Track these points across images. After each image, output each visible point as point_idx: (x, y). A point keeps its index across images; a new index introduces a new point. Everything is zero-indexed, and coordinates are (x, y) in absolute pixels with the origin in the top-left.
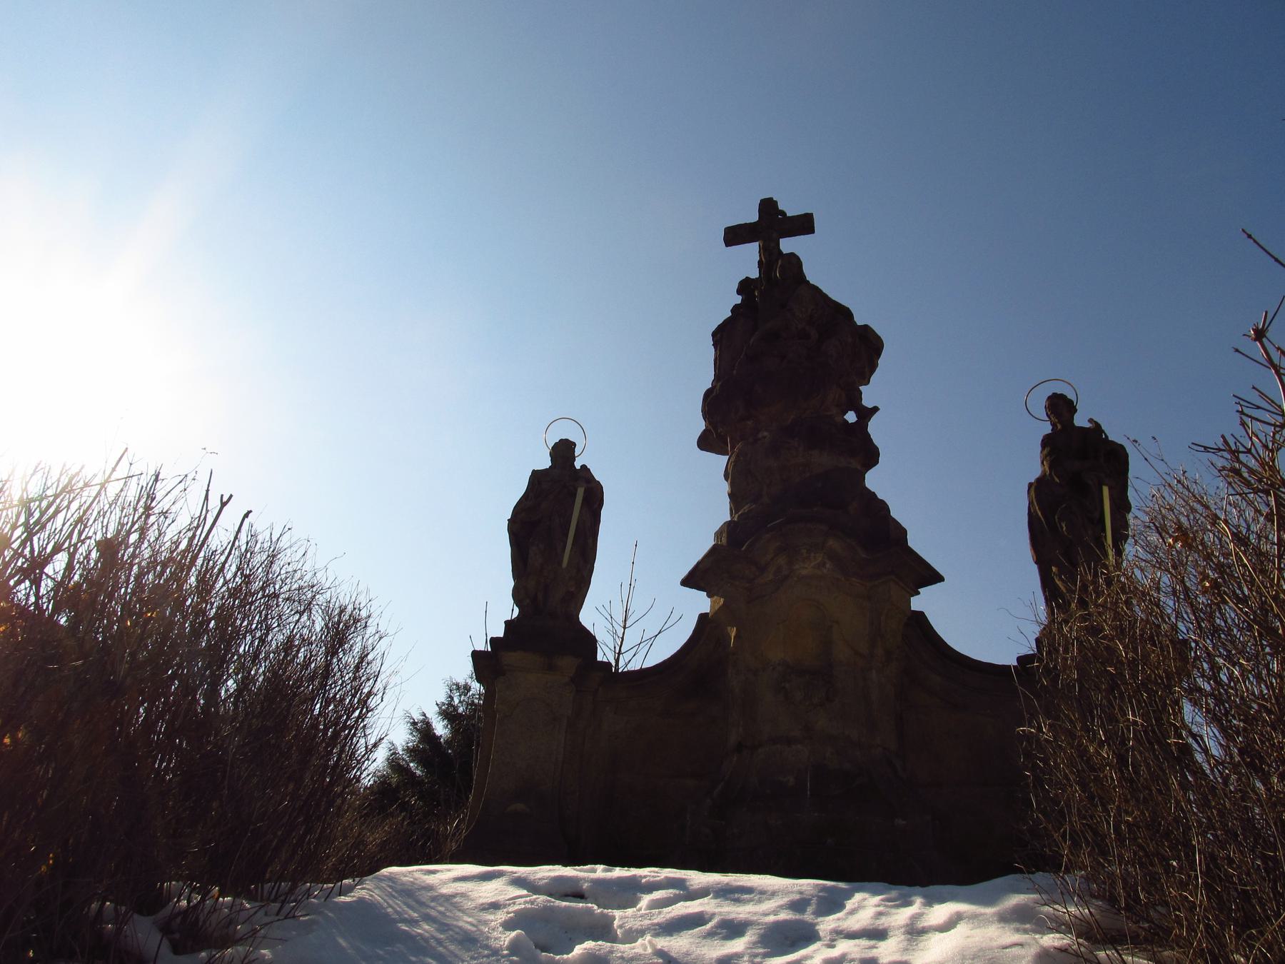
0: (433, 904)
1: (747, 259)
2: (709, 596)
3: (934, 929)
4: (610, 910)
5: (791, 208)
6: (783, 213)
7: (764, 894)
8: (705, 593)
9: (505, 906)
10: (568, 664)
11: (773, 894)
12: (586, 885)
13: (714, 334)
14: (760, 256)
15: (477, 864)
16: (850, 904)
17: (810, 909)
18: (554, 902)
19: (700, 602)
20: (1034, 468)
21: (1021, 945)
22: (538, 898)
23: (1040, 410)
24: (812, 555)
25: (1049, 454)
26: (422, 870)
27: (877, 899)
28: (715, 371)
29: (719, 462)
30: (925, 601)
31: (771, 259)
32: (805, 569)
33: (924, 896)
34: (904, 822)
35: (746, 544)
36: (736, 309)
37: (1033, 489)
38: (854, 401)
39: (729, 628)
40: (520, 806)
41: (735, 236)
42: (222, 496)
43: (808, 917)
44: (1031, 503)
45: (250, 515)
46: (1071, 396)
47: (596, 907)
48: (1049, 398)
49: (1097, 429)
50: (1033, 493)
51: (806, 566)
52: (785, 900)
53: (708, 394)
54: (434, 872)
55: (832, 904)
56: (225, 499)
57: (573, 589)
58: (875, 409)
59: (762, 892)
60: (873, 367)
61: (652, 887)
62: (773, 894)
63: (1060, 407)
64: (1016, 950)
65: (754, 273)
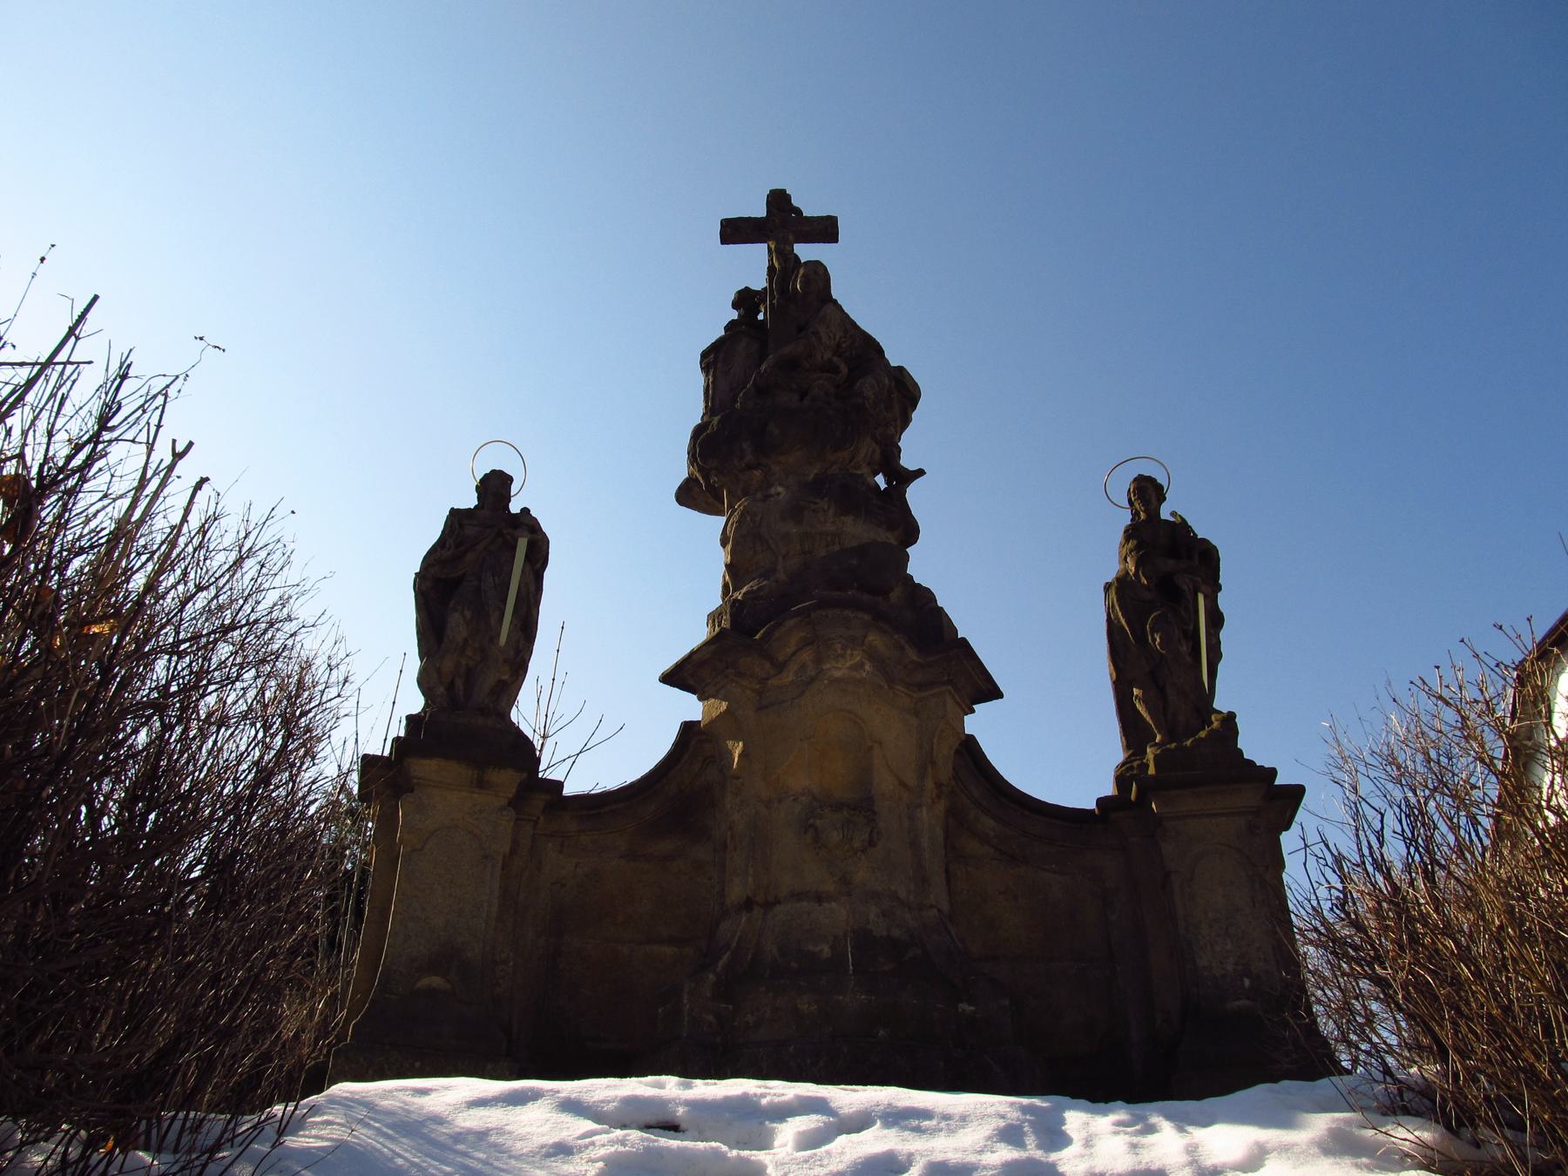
0: (460, 1147)
2: (700, 699)
3: (1231, 1169)
4: (754, 1152)
5: (810, 205)
6: (798, 211)
9: (581, 1149)
10: (507, 780)
11: (964, 1119)
12: (681, 1111)
13: (705, 355)
14: (771, 260)
15: (439, 1077)
19: (690, 707)
22: (629, 1135)
24: (849, 652)
25: (1137, 548)
26: (405, 1089)
28: (706, 401)
30: (981, 723)
31: (784, 268)
32: (838, 669)
34: (973, 1008)
35: (762, 632)
36: (731, 326)
37: (1113, 591)
38: (888, 459)
39: (730, 743)
40: (436, 981)
41: (735, 231)
42: (174, 441)
45: (205, 486)
46: (1162, 480)
47: (724, 1148)
48: (1135, 480)
51: (840, 666)
53: (698, 432)
54: (424, 1092)
56: (179, 449)
57: (505, 677)
58: (920, 473)
59: (946, 1117)
61: (783, 1112)
62: (964, 1119)
63: (1147, 492)
65: (759, 282)
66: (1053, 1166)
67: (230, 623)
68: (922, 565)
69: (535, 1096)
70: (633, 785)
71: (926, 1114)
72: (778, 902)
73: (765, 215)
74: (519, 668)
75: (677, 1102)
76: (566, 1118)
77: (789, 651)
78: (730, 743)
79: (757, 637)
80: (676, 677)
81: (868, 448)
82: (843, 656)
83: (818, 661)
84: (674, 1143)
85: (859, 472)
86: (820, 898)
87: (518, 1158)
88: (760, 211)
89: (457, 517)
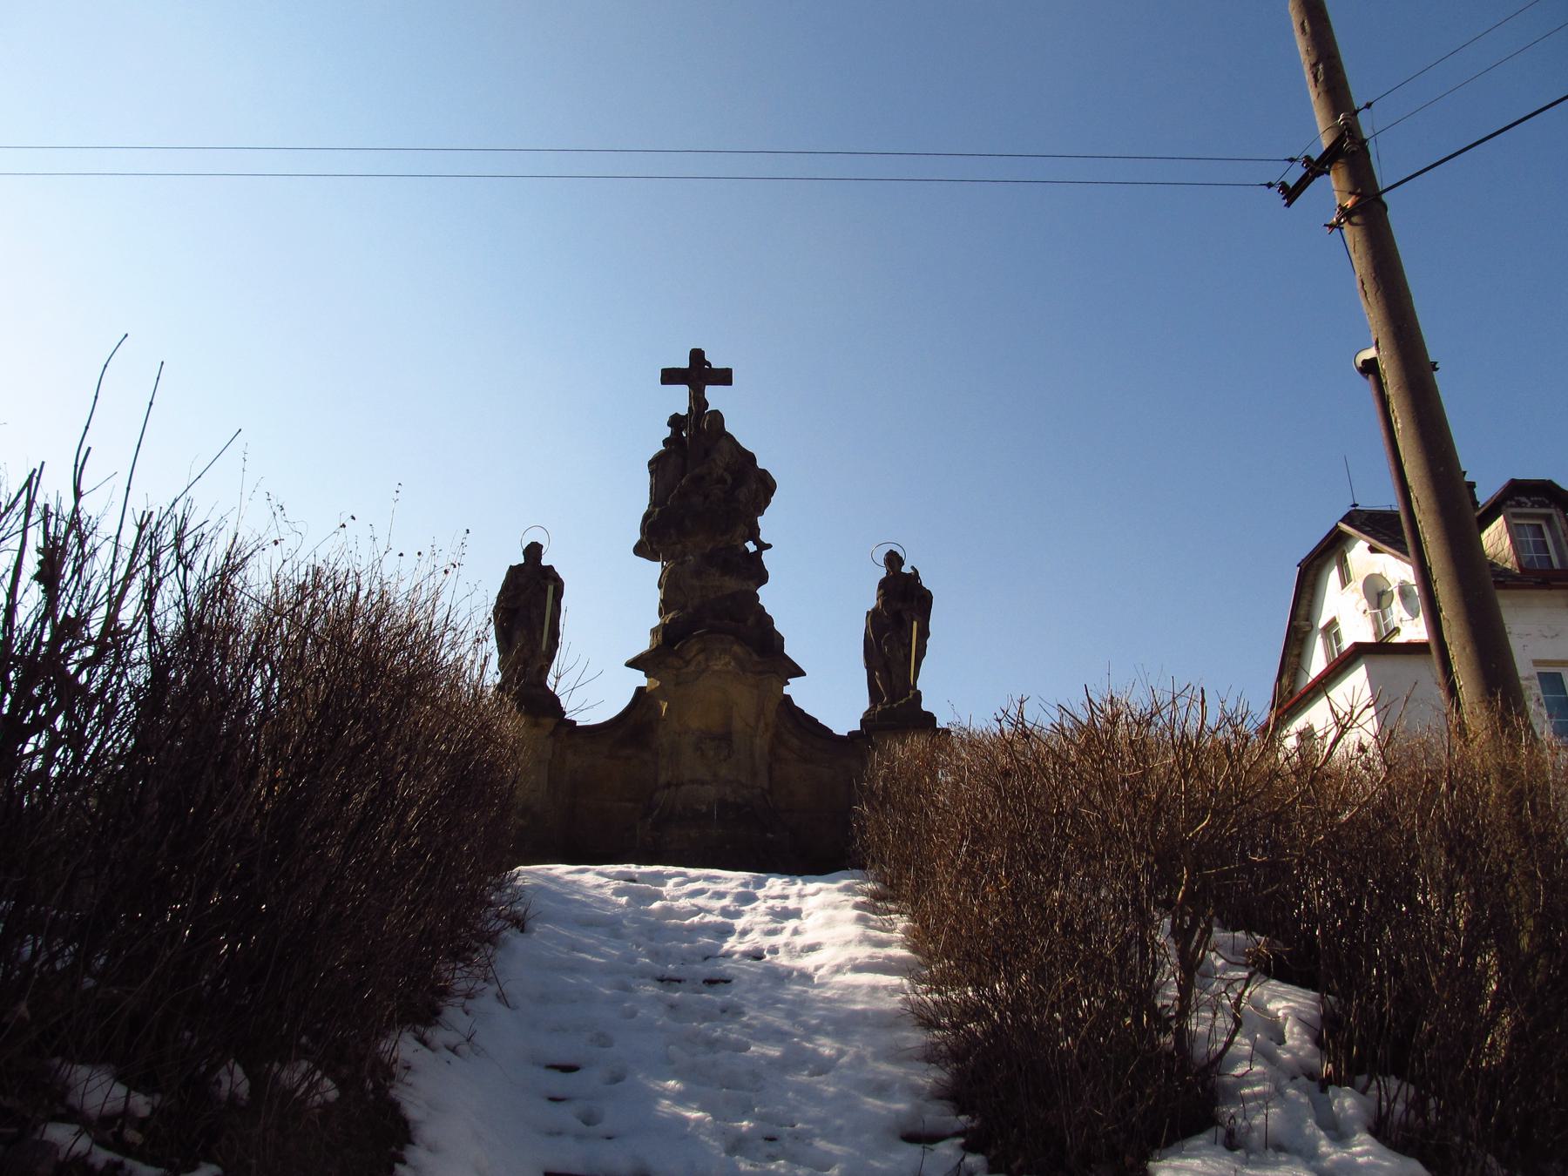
1: (679, 399)
2: (646, 676)
5: (716, 361)
7: (726, 880)
8: (643, 673)
10: (549, 722)
11: (731, 879)
12: (637, 875)
13: (650, 463)
14: (690, 403)
16: (768, 884)
17: (751, 887)
18: (399, 897)
19: (639, 679)
20: (871, 600)
21: (847, 901)
23: (880, 558)
24: (722, 656)
25: (883, 595)
27: (780, 881)
29: (654, 569)
30: (795, 690)
31: (698, 401)
32: (717, 666)
33: (802, 881)
38: (754, 534)
41: (670, 376)
43: (751, 889)
44: (867, 627)
46: (901, 554)
49: (915, 576)
50: (869, 619)
52: (738, 882)
53: (646, 517)
55: (760, 884)
59: (726, 879)
60: (767, 503)
61: (671, 876)
62: (731, 879)
63: (893, 560)
64: (845, 902)
65: (684, 411)
66: (755, 894)
67: (827, 1034)
68: (767, 596)
69: (588, 870)
70: (611, 721)
71: (719, 878)
72: (683, 784)
73: (688, 367)
74: (551, 657)
75: (636, 873)
76: (600, 878)
77: (692, 654)
78: (661, 702)
79: (676, 648)
80: (633, 664)
81: (742, 529)
82: (720, 658)
83: (707, 660)
84: (635, 885)
85: (736, 544)
86: (703, 783)
87: (588, 888)
88: (685, 364)
89: (513, 571)
